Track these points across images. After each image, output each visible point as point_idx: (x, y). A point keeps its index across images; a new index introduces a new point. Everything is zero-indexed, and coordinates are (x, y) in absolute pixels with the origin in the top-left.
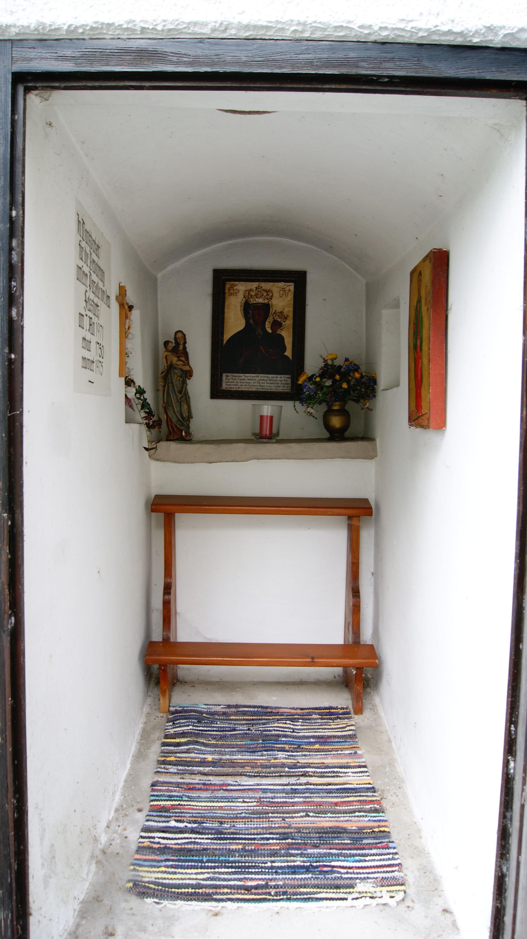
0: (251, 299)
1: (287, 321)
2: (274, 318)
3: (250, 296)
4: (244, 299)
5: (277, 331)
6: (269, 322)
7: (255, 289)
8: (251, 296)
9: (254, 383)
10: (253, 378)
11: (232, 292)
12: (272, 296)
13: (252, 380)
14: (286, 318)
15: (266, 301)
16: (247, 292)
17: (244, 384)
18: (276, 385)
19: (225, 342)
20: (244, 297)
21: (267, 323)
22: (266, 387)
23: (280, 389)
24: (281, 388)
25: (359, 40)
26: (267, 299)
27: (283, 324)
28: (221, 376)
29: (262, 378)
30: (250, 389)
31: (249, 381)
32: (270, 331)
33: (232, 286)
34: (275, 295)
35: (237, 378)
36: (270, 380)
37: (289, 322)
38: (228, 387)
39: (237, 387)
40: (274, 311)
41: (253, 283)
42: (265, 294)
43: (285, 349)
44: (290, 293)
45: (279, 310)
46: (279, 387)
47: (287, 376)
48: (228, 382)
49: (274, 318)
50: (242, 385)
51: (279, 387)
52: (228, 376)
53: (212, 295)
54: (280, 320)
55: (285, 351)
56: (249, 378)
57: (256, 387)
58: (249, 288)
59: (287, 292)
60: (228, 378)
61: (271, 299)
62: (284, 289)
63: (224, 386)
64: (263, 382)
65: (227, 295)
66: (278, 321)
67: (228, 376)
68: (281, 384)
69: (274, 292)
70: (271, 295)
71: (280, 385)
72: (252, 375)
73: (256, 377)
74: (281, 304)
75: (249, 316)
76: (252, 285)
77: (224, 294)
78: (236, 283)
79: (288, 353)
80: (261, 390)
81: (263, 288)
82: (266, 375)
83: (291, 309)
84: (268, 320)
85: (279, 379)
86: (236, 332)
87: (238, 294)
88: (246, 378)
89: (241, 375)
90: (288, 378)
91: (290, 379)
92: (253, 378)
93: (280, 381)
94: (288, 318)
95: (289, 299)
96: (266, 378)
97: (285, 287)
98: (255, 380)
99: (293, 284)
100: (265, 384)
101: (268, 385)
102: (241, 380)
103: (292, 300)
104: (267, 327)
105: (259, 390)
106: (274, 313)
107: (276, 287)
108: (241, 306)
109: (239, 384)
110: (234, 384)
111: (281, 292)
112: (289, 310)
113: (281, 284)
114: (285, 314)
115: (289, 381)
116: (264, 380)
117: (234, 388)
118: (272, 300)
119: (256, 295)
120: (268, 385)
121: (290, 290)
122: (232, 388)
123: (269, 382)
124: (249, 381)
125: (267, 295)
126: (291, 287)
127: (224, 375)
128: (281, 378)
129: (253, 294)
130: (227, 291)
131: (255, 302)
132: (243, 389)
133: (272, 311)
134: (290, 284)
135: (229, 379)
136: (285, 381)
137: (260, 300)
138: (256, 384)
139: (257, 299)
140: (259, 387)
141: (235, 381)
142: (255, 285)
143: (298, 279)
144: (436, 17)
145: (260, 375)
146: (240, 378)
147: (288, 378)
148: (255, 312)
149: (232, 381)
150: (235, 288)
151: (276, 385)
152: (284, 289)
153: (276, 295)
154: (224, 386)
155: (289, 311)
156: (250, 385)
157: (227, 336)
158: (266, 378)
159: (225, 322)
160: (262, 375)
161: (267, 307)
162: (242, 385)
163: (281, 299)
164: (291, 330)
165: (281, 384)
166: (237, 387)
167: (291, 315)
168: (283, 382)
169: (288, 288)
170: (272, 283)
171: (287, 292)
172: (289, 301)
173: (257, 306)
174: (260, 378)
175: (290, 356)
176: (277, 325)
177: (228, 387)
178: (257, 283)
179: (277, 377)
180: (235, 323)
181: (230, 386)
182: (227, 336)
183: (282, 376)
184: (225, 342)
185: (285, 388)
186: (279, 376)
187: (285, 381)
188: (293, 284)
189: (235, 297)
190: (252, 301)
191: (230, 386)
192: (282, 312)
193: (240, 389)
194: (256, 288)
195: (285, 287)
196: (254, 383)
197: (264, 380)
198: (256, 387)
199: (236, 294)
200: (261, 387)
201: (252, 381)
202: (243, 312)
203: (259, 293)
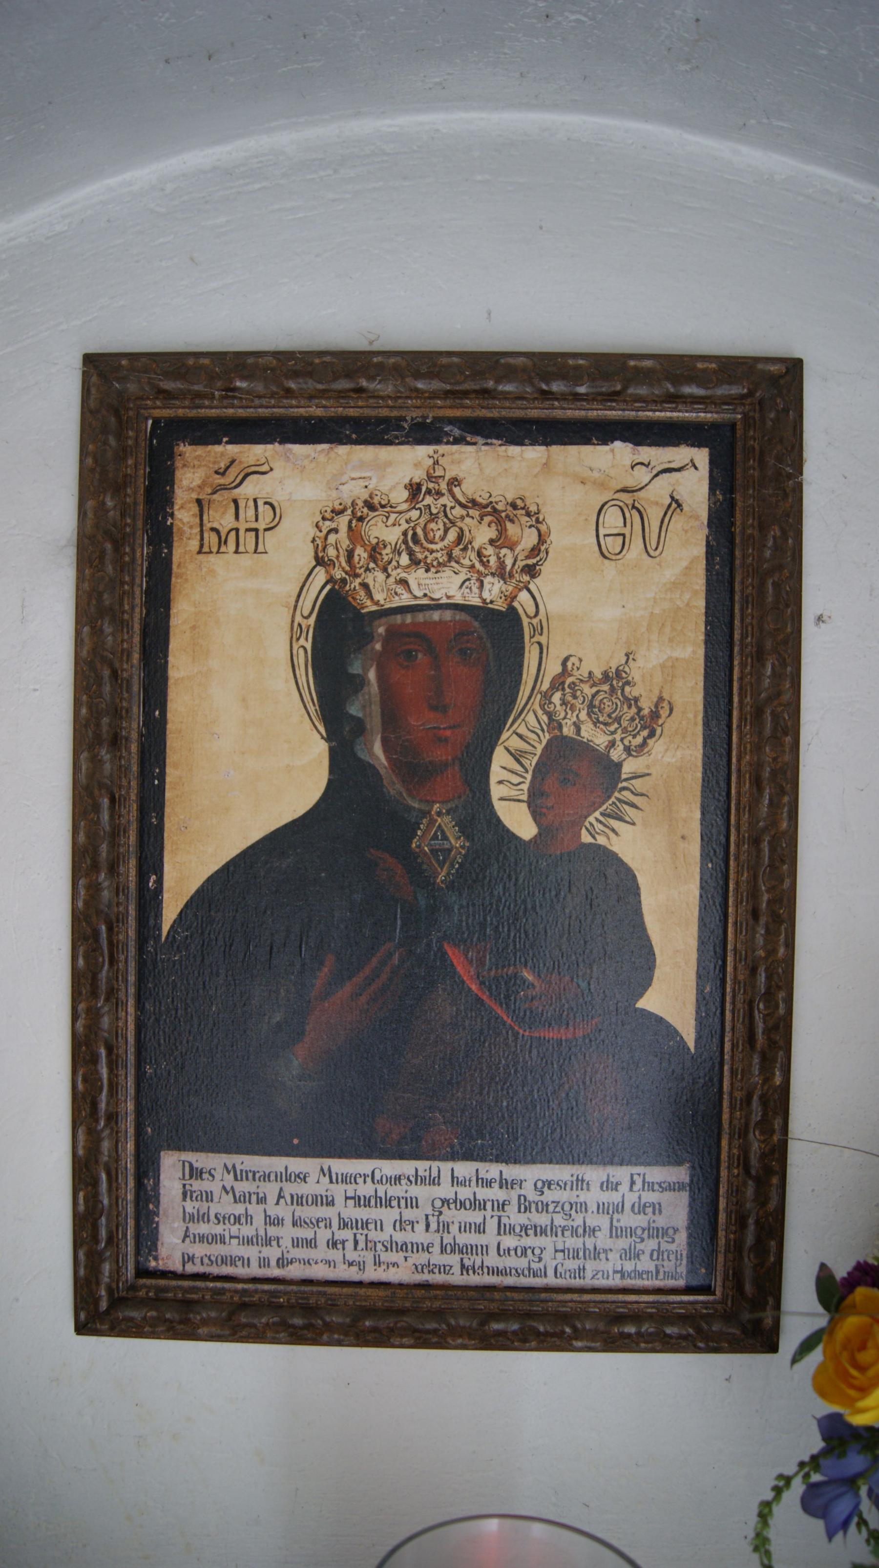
0: (375, 580)
1: (657, 747)
2: (554, 724)
3: (361, 553)
4: (320, 576)
5: (578, 823)
6: (517, 756)
7: (400, 496)
8: (374, 552)
9: (401, 1224)
10: (395, 1191)
11: (226, 521)
12: (535, 551)
13: (387, 1202)
14: (650, 723)
15: (493, 591)
16: (343, 522)
17: (324, 1235)
18: (572, 1242)
19: (170, 912)
20: (320, 561)
21: (500, 759)
22: (492, 1260)
23: (606, 1270)
24: (614, 1262)
25: (597, 510)
26: (502, 573)
27: (628, 768)
28: (147, 1169)
29: (465, 1193)
30: (372, 1274)
31: (362, 1214)
32: (521, 823)
33: (227, 480)
34: (557, 541)
35: (271, 1189)
36: (524, 1206)
37: (673, 761)
38: (199, 1250)
39: (273, 1253)
40: (553, 668)
41: (384, 453)
42: (483, 534)
43: (642, 964)
44: (677, 523)
45: (593, 662)
46: (596, 1254)
47: (657, 1174)
48: (203, 1217)
49: (554, 724)
50: (311, 1243)
51: (596, 1254)
52: (196, 1173)
53: (72, 551)
54: (600, 740)
55: (645, 983)
56: (365, 1189)
57: (421, 1258)
58: (353, 491)
59: (654, 516)
60: (197, 1185)
61: (532, 571)
62: (629, 500)
63: (173, 1248)
64: (476, 1217)
65: (183, 550)
66: (586, 749)
67: (196, 1173)
68: (615, 1232)
69: (553, 521)
70: (529, 539)
71: (602, 1240)
72: (389, 1167)
73: (417, 1179)
74: (607, 615)
75: (354, 710)
76: (382, 467)
77: (162, 536)
78: (256, 452)
79: (672, 996)
80: (456, 1278)
81: (469, 488)
82: (492, 1170)
83: (691, 649)
84: (509, 739)
85: (593, 1196)
86: (256, 835)
87: (270, 540)
88: (338, 1191)
89: (297, 1164)
90: (671, 1187)
91: (684, 1198)
92: (395, 1191)
93: (601, 1208)
94: (669, 725)
95: (669, 574)
96: (496, 1193)
97: (642, 475)
98: (412, 1203)
99: (701, 456)
100: (490, 1238)
101: (509, 1242)
102: (299, 1200)
103: (699, 582)
104: (496, 791)
105: (438, 1278)
106: (558, 683)
107: (565, 485)
108: (295, 632)
109: (287, 1233)
110: (247, 1231)
111: (612, 520)
112: (673, 663)
113: (615, 458)
114: (644, 692)
115: (677, 1211)
116: (477, 1204)
117: (252, 1261)
118: (537, 584)
119: (412, 540)
120: (509, 1242)
121: (676, 503)
122: (232, 1261)
123: (514, 1217)
124: (362, 1214)
125: (500, 541)
126: (689, 476)
127: (171, 1165)
128: (610, 1185)
129: (392, 535)
130: (183, 516)
131: (405, 599)
132: (320, 1272)
133: (537, 668)
134: (681, 454)
135: (209, 1197)
136: (641, 1208)
137: (448, 586)
138: (419, 1235)
139: (417, 577)
140: (437, 1258)
141: (256, 1210)
142: (406, 462)
143: (743, 425)
144: (682, 510)
145: (446, 1167)
146: (290, 1189)
147: (671, 1187)
148: (409, 681)
149: (225, 1209)
150: (249, 489)
151: (572, 1242)
152: (629, 500)
153: (569, 537)
154: (173, 1248)
155: (670, 668)
156: (370, 1245)
157: (189, 866)
158: (496, 1193)
159: (171, 758)
160: (464, 1169)
161: (499, 636)
162: (311, 1243)
163: (607, 578)
164: (690, 815)
165: (615, 1232)
166: (273, 1253)
167: (689, 695)
168: (628, 1220)
169: (659, 491)
170: (534, 453)
171: (654, 516)
172: (675, 586)
173: (416, 636)
174: (445, 1190)
175: (686, 1026)
176: (575, 774)
177: (199, 1250)
178: (423, 452)
179: (580, 1183)
180: (249, 763)
181: (217, 1250)
182: (189, 866)
183: (621, 1173)
184: (170, 912)
185: (646, 1264)
186: (594, 1174)
187: (641, 1208)
188: (701, 456)
189: (246, 561)
190: (380, 591)
191: (217, 1250)
192: (615, 679)
193: (294, 1272)
194: (415, 490)
195: (642, 475)
196: (401, 1224)
197: (477, 1204)
198: (421, 1258)
199: (252, 536)
200: (453, 1260)
201: (389, 1215)
202: (307, 677)
203: (437, 528)
